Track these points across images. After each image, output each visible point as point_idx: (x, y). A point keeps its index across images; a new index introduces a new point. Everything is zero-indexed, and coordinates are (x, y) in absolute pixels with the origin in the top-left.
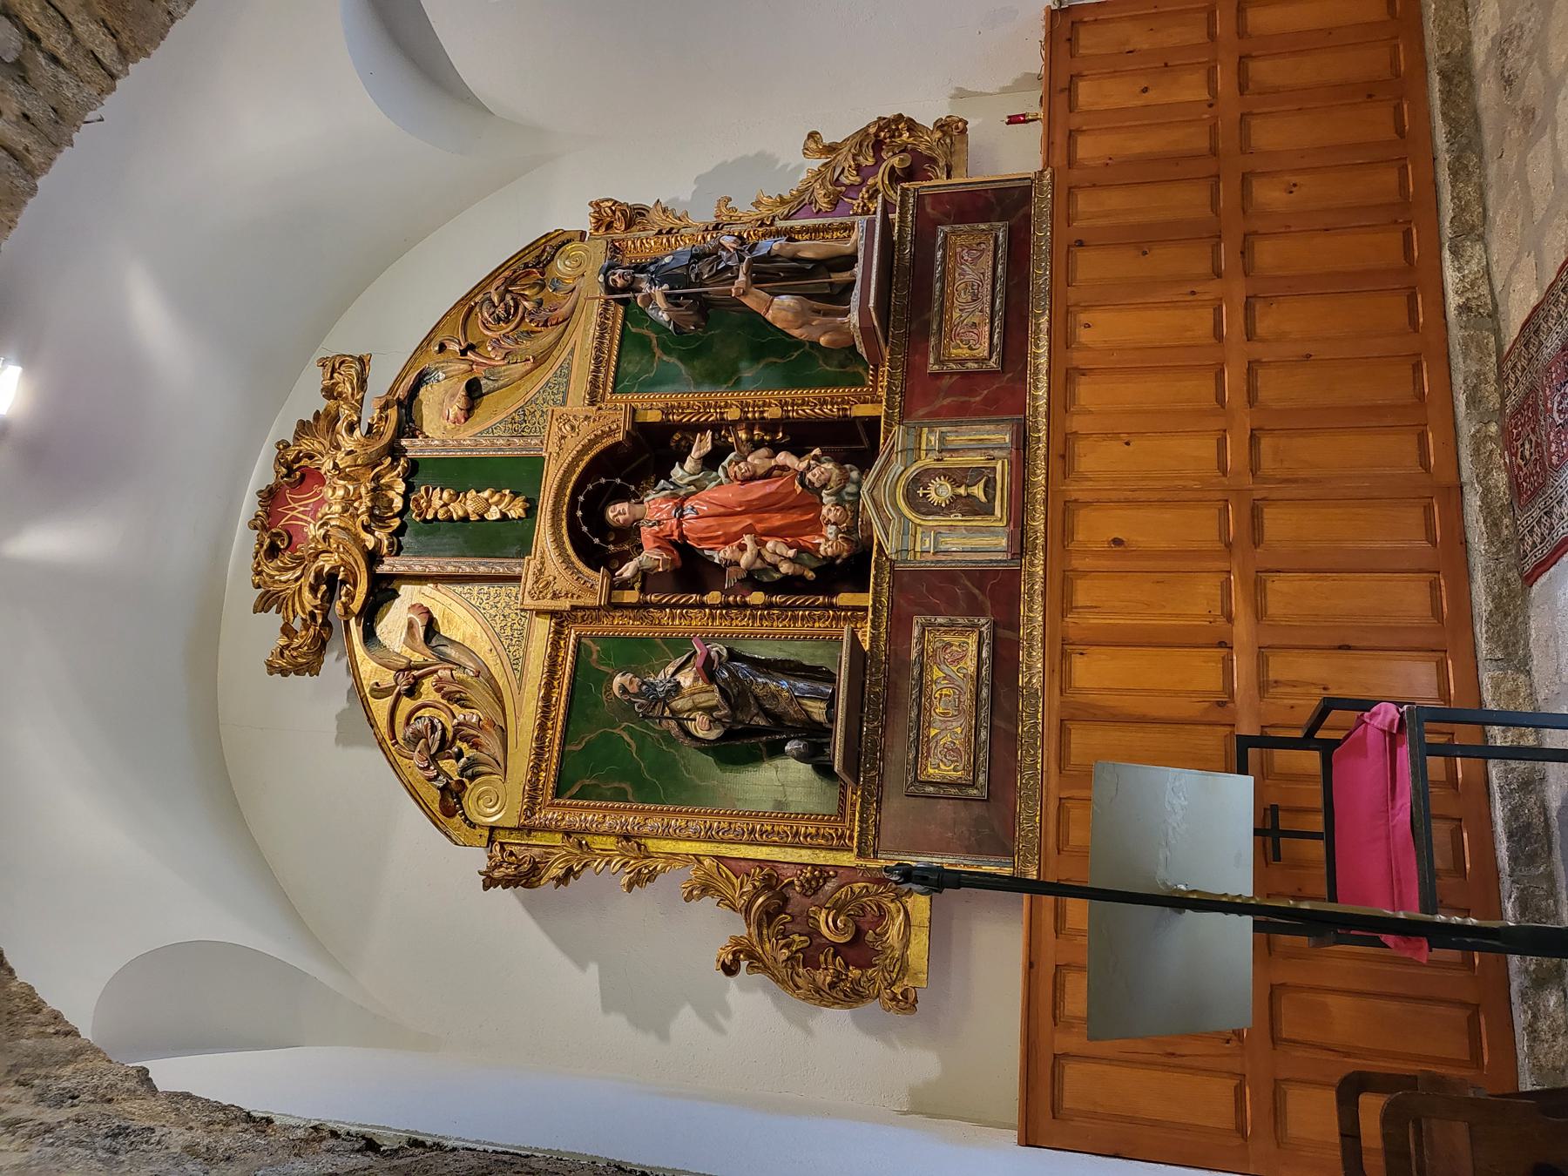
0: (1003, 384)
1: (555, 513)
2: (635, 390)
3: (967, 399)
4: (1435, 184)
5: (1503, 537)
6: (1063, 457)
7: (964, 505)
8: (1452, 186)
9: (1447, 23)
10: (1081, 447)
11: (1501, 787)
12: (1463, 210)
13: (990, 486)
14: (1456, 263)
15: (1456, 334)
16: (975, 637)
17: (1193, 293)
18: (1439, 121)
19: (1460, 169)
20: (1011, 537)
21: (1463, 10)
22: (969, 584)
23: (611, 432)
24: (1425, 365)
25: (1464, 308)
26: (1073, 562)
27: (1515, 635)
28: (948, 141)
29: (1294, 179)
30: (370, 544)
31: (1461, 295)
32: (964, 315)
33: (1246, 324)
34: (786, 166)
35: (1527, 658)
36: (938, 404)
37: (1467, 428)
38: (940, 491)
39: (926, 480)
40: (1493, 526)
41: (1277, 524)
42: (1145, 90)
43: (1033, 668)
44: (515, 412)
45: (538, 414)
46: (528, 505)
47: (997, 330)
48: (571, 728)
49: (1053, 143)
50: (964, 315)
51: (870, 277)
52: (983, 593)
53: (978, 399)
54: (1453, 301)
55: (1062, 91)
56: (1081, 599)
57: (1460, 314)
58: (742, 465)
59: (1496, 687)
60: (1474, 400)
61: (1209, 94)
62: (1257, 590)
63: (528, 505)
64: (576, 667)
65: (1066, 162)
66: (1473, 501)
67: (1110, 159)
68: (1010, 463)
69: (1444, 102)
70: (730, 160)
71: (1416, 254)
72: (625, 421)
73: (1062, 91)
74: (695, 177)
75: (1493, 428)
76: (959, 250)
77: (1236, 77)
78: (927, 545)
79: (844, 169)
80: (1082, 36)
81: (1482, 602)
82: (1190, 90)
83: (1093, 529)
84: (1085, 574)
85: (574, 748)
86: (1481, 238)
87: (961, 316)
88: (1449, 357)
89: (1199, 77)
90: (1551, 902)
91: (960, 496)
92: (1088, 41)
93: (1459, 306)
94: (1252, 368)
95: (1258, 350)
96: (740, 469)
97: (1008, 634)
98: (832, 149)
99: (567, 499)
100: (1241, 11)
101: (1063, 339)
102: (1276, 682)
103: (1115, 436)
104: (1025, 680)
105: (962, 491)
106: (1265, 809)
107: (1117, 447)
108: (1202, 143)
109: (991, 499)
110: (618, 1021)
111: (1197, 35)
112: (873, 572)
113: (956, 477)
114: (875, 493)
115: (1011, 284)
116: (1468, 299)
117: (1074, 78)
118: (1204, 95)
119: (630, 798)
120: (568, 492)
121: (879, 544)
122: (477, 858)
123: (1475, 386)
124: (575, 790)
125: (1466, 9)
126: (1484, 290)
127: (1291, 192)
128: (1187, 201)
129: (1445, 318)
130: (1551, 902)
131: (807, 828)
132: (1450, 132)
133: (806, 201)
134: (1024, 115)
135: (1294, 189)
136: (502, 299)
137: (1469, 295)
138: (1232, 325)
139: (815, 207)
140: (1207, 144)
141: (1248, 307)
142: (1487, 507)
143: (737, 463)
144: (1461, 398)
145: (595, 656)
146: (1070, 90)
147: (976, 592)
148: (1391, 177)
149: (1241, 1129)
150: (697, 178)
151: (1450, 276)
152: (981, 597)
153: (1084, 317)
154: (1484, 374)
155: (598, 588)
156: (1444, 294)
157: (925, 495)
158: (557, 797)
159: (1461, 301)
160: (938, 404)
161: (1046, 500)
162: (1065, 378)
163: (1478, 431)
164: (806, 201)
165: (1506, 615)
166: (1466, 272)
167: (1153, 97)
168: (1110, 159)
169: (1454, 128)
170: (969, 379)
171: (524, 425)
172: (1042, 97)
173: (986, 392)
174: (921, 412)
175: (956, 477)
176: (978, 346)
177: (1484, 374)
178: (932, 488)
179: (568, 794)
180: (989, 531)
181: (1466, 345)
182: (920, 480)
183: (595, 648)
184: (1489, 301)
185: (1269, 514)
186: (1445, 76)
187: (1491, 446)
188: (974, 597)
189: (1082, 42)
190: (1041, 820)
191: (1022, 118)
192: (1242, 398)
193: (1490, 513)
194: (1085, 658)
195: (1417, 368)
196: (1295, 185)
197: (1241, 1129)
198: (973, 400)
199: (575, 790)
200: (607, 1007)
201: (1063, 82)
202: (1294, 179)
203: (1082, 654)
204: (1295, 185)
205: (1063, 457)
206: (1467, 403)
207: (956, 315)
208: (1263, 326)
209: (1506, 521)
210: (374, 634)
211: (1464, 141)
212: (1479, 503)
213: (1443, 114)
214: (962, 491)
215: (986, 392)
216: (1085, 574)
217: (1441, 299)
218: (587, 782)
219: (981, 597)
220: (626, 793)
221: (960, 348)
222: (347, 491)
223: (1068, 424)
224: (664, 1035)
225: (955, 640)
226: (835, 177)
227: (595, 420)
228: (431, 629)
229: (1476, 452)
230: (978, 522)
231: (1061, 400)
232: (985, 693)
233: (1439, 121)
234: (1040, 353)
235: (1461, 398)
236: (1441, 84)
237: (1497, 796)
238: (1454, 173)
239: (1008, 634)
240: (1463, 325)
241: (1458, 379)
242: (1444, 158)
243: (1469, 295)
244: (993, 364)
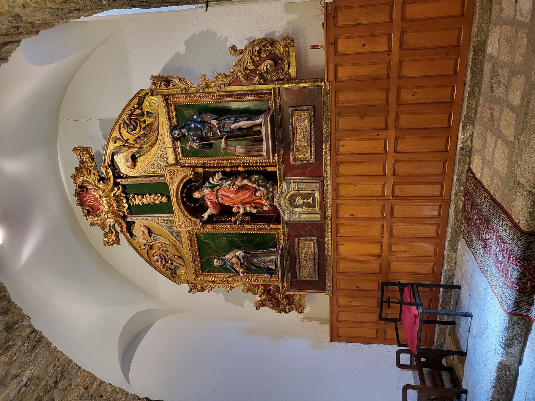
0: (316, 166)
1: (178, 202)
2: (190, 155)
3: (304, 171)
4: (463, 95)
5: (458, 219)
6: (336, 189)
7: (306, 205)
8: (468, 101)
9: (481, 25)
10: (341, 187)
11: (444, 278)
12: (469, 111)
13: (314, 199)
14: (463, 132)
15: (458, 157)
16: (313, 242)
17: (378, 135)
18: (469, 73)
19: (472, 94)
20: (321, 215)
21: (489, 19)
22: (309, 227)
23: (187, 176)
24: (447, 163)
25: (462, 148)
26: (339, 221)
27: (455, 244)
28: (287, 49)
29: (415, 90)
30: (122, 214)
31: (462, 144)
32: (301, 142)
33: (394, 145)
34: (220, 37)
35: (456, 250)
36: (295, 172)
37: (455, 187)
38: (299, 201)
39: (294, 197)
40: (456, 216)
41: (399, 211)
42: (364, 45)
43: (329, 249)
44: (151, 165)
45: (159, 165)
46: (167, 199)
47: (313, 150)
48: (201, 256)
49: (329, 70)
50: (301, 142)
51: (268, 125)
52: (314, 229)
53: (308, 171)
54: (459, 145)
55: (332, 44)
56: (342, 231)
57: (460, 150)
58: (234, 187)
59: (448, 256)
60: (458, 179)
61: (388, 48)
62: (391, 226)
63: (167, 199)
64: (200, 258)
65: (334, 79)
66: (452, 209)
67: (351, 77)
68: (319, 192)
69: (472, 63)
70: (197, 33)
71: (452, 123)
72: (192, 173)
73: (332, 44)
74: (184, 42)
75: (462, 188)
76: (297, 117)
77: (399, 41)
78: (296, 217)
79: (247, 62)
80: (339, 15)
81: (449, 235)
82: (374, 231)
83: (345, 212)
84: (342, 224)
85: (203, 261)
86: (473, 122)
87: (300, 143)
88: (455, 161)
89: (385, 40)
90: (449, 300)
91: (305, 202)
92: (343, 19)
93: (461, 147)
94: (395, 162)
95: (398, 156)
96: (234, 189)
97: (322, 240)
98: (242, 52)
99: (180, 197)
100: (404, 4)
101: (335, 152)
102: (393, 251)
103: (352, 184)
104: (325, 146)
105: (305, 201)
106: (385, 324)
107: (352, 187)
108: (384, 72)
109: (314, 203)
110: (230, 305)
111: (384, 18)
112: (278, 177)
113: (304, 196)
114: (279, 201)
115: (317, 129)
116: (464, 145)
117: (336, 38)
118: (387, 49)
119: (223, 272)
120: (180, 195)
121: (282, 217)
122: (186, 287)
123: (460, 175)
124: (207, 270)
125: (490, 19)
126: (469, 142)
127: (414, 96)
128: (378, 97)
129: (456, 147)
130: (449, 300)
131: (259, 160)
132: (472, 78)
133: (235, 77)
134: (317, 46)
135: (415, 94)
136: (131, 122)
137: (464, 144)
138: (390, 148)
139: (239, 80)
140: (386, 73)
141: (396, 140)
142: (455, 211)
143: (233, 186)
144: (455, 178)
145: (202, 238)
146: (335, 44)
147: (312, 229)
148: (448, 91)
149: (377, 337)
150: (185, 42)
151: (460, 136)
152: (313, 230)
153: (341, 143)
154: (463, 171)
155: (199, 224)
156: (457, 139)
157: (294, 202)
158: (203, 272)
159: (462, 146)
160: (295, 172)
161: (331, 232)
162: (336, 165)
163: (458, 189)
164: (235, 77)
165: (454, 239)
166: (465, 136)
167: (367, 49)
168: (351, 77)
169: (473, 73)
170: (304, 167)
171: (156, 169)
172: (323, 23)
173: (310, 168)
174: (290, 175)
175: (304, 196)
176: (307, 154)
177: (463, 171)
178: (296, 200)
179: (205, 271)
180: (316, 213)
181: (460, 161)
182: (291, 197)
183: (202, 236)
184: (470, 147)
185: (396, 207)
186: (475, 52)
187: (460, 193)
188: (312, 230)
189: (339, 19)
190: (330, 96)
191: (316, 47)
192: (391, 172)
193: (456, 212)
194: (343, 246)
195: (445, 163)
196: (416, 93)
197: (377, 337)
198: (306, 171)
199: (207, 270)
200: (227, 302)
201: (332, 40)
202: (415, 90)
203: (342, 245)
204: (416, 93)
205: (336, 190)
206: (457, 180)
207: (298, 143)
208: (400, 148)
209: (460, 215)
210: (133, 234)
211: (476, 81)
212: (454, 209)
213: (471, 69)
214: (305, 201)
215: (310, 168)
216: (342, 224)
217: (458, 128)
218: (210, 269)
219: (313, 230)
220: (221, 271)
221: (301, 154)
222: (107, 201)
223: (337, 180)
224: (243, 306)
225: (307, 242)
226: (245, 66)
227: (181, 171)
228: (150, 232)
229: (456, 194)
230: (310, 210)
231: (336, 174)
232: (316, 256)
233: (469, 73)
234: (327, 158)
235: (455, 178)
236: (473, 55)
237: (443, 279)
238: (469, 96)
239: (322, 240)
240: (461, 153)
241: (456, 170)
242: (468, 89)
243: (464, 144)
244: (315, 239)
